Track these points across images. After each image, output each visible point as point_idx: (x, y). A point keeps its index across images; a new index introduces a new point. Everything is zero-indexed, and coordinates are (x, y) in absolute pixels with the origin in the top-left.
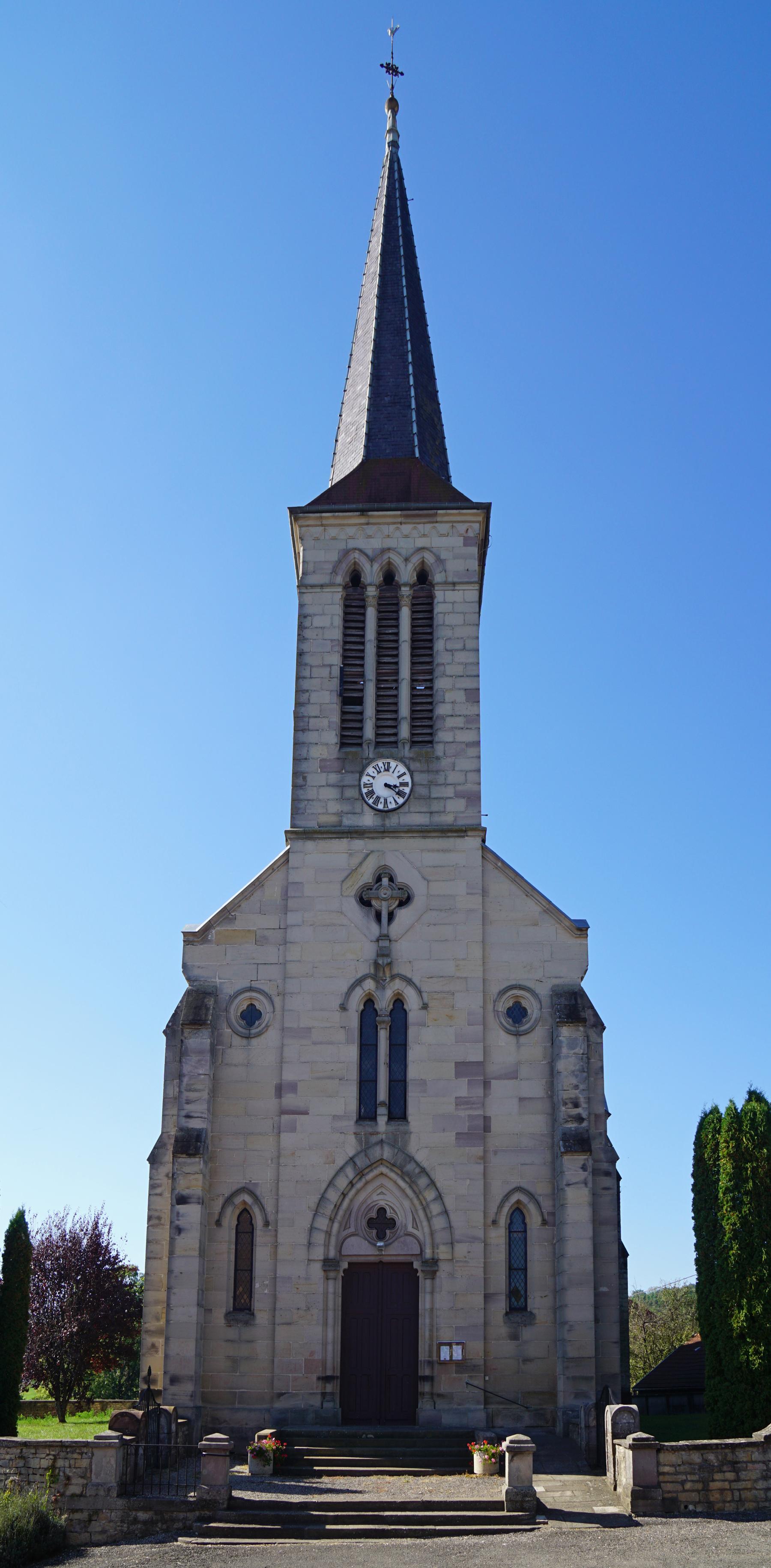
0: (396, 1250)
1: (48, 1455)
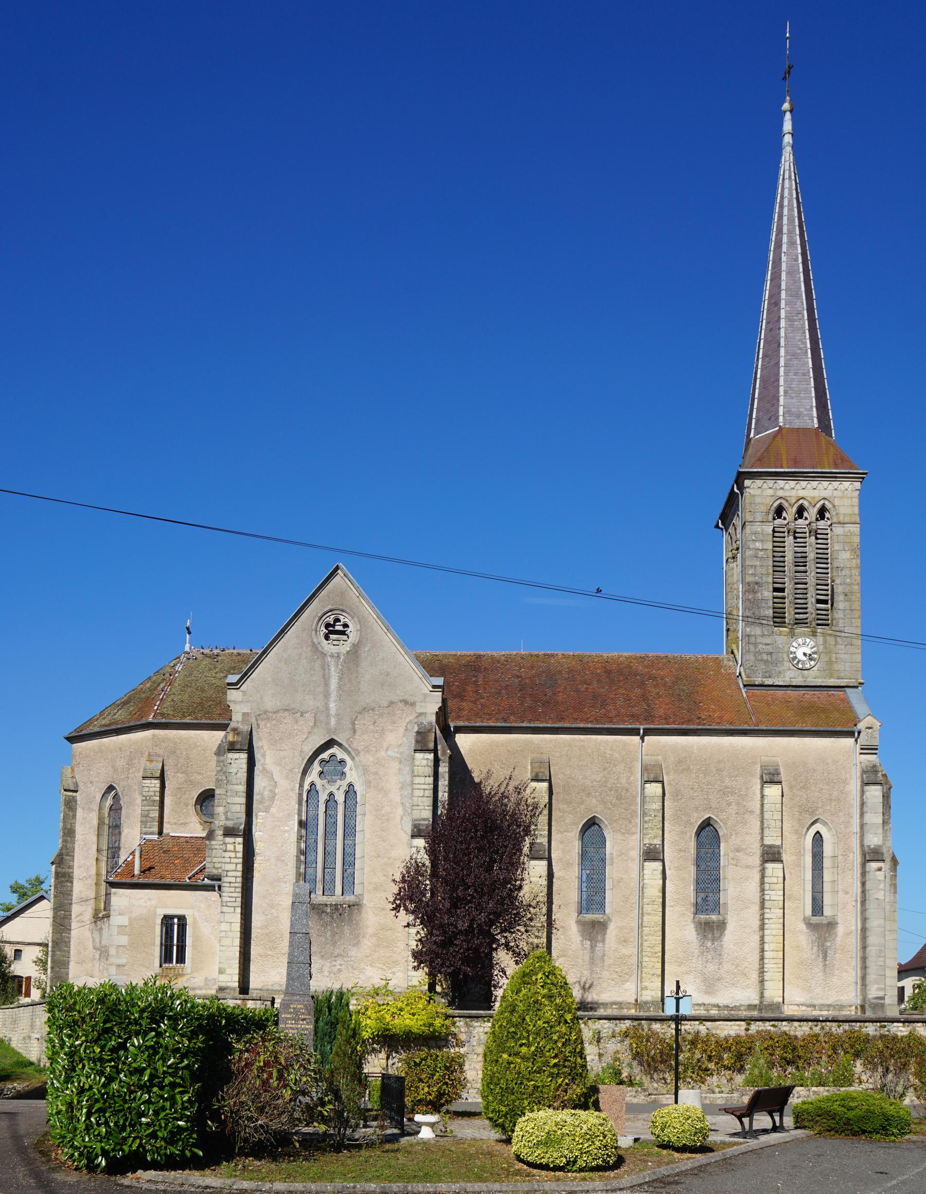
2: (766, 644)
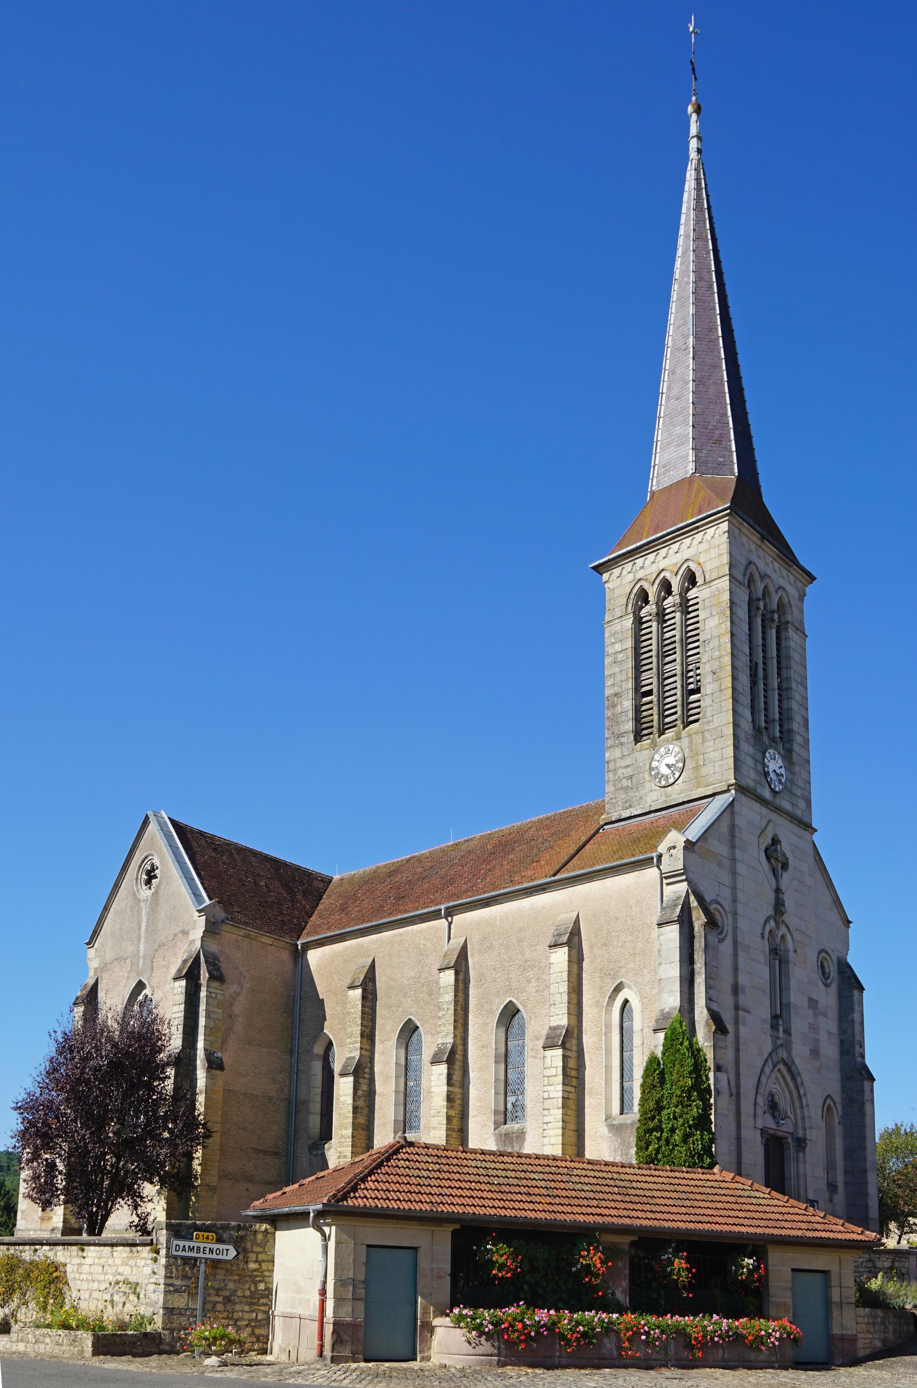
0: (787, 1127)
2: (627, 767)
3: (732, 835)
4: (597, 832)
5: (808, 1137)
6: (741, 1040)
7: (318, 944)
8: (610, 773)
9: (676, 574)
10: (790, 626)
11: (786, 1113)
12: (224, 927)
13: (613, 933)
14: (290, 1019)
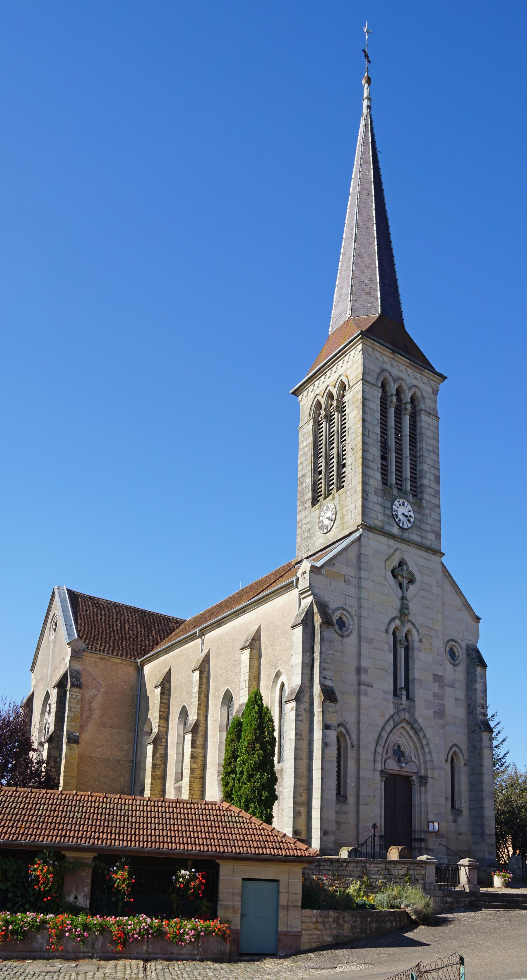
0: (407, 769)
1: (403, 868)
2: (308, 523)
3: (359, 561)
4: (290, 570)
5: (429, 775)
6: (362, 707)
7: (148, 661)
8: (299, 529)
9: (335, 387)
10: (422, 412)
11: (411, 758)
12: (85, 654)
13: (276, 637)
14: (134, 710)
